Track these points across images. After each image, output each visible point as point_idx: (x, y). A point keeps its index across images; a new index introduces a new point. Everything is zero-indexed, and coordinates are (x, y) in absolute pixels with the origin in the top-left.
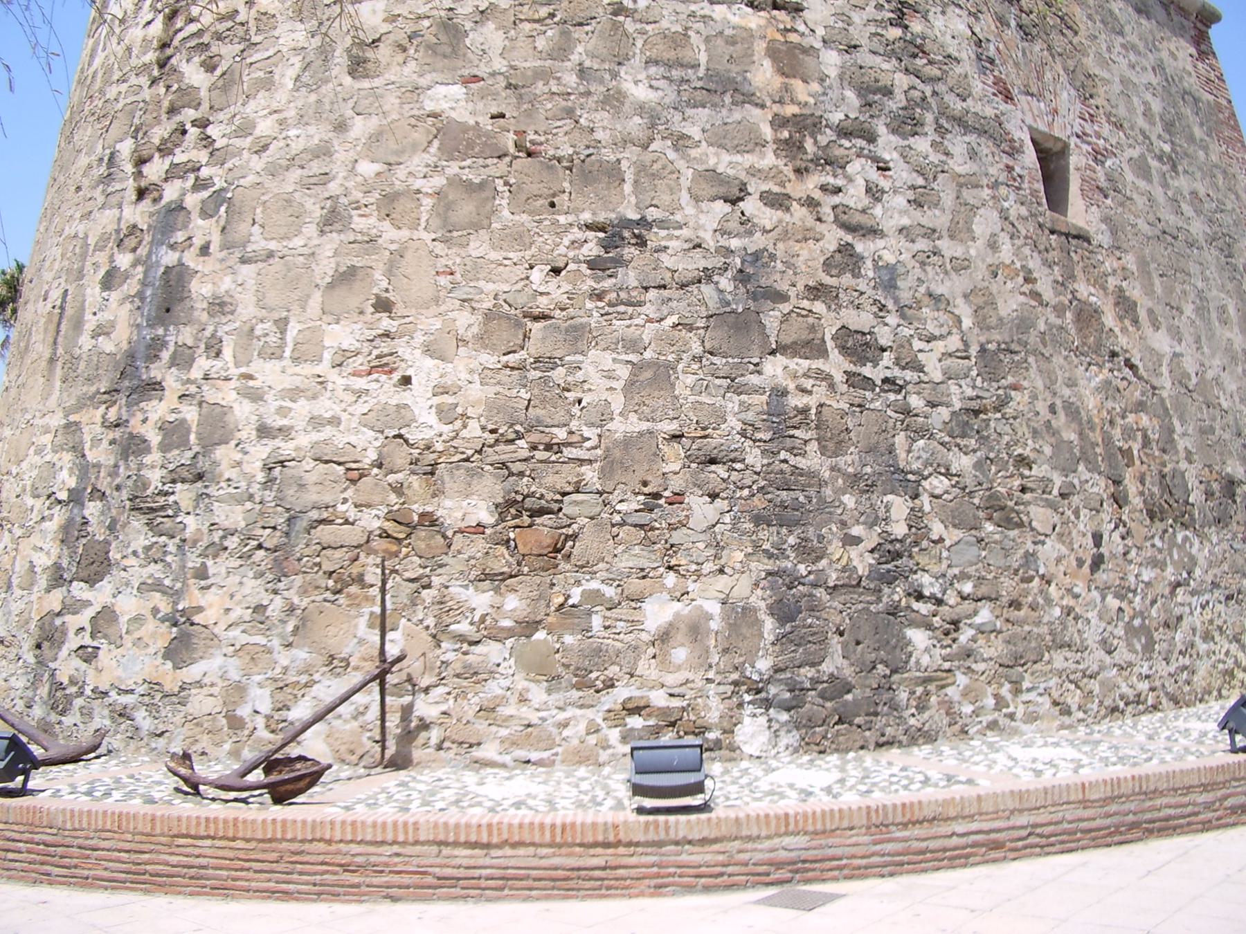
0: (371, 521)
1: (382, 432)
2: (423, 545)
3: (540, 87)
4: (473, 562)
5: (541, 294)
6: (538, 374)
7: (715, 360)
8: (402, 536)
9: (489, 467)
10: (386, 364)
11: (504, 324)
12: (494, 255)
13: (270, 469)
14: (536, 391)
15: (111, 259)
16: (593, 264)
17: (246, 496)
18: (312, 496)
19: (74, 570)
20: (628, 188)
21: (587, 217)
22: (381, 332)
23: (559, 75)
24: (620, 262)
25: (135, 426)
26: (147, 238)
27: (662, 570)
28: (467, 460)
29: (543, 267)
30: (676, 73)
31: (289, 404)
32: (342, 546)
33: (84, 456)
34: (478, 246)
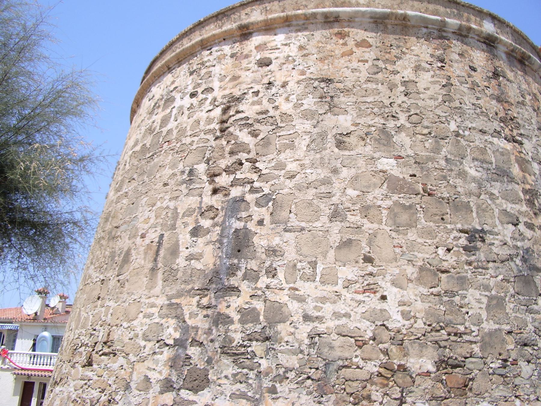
0: (372, 367)
1: (374, 323)
2: (401, 381)
3: (430, 165)
4: (427, 391)
5: (444, 260)
6: (447, 299)
7: (520, 297)
8: (389, 376)
9: (429, 343)
10: (373, 289)
11: (429, 274)
12: (420, 240)
13: (312, 338)
14: (447, 307)
15: (197, 221)
16: (465, 248)
17: (298, 351)
18: (338, 353)
19: (182, 383)
20: (474, 214)
21: (459, 226)
22: (368, 272)
23: (437, 160)
24: (476, 249)
25: (222, 308)
26: (221, 214)
27: (513, 397)
28: (418, 339)
29: (443, 248)
30: (485, 165)
31: (321, 305)
32: (357, 380)
33: (184, 322)
34: (412, 235)
